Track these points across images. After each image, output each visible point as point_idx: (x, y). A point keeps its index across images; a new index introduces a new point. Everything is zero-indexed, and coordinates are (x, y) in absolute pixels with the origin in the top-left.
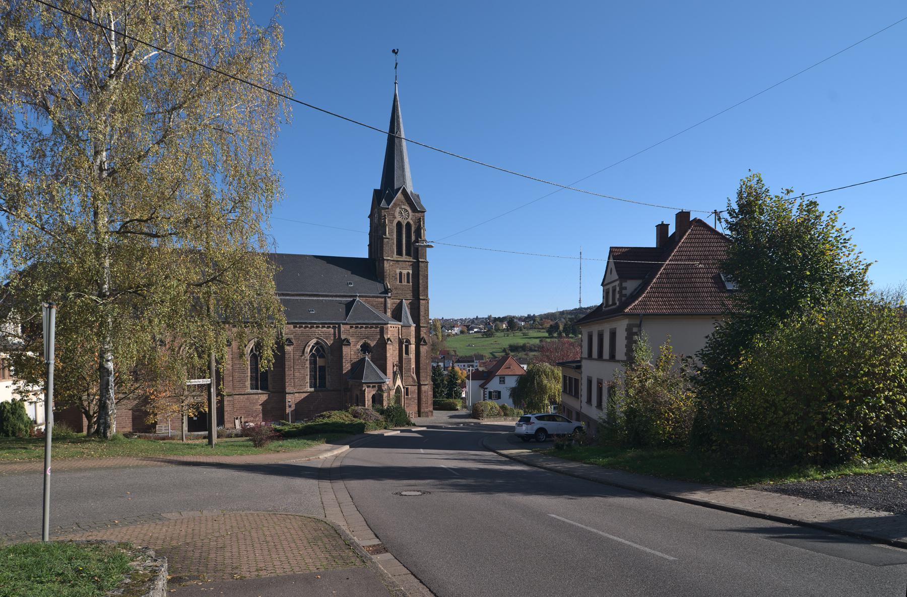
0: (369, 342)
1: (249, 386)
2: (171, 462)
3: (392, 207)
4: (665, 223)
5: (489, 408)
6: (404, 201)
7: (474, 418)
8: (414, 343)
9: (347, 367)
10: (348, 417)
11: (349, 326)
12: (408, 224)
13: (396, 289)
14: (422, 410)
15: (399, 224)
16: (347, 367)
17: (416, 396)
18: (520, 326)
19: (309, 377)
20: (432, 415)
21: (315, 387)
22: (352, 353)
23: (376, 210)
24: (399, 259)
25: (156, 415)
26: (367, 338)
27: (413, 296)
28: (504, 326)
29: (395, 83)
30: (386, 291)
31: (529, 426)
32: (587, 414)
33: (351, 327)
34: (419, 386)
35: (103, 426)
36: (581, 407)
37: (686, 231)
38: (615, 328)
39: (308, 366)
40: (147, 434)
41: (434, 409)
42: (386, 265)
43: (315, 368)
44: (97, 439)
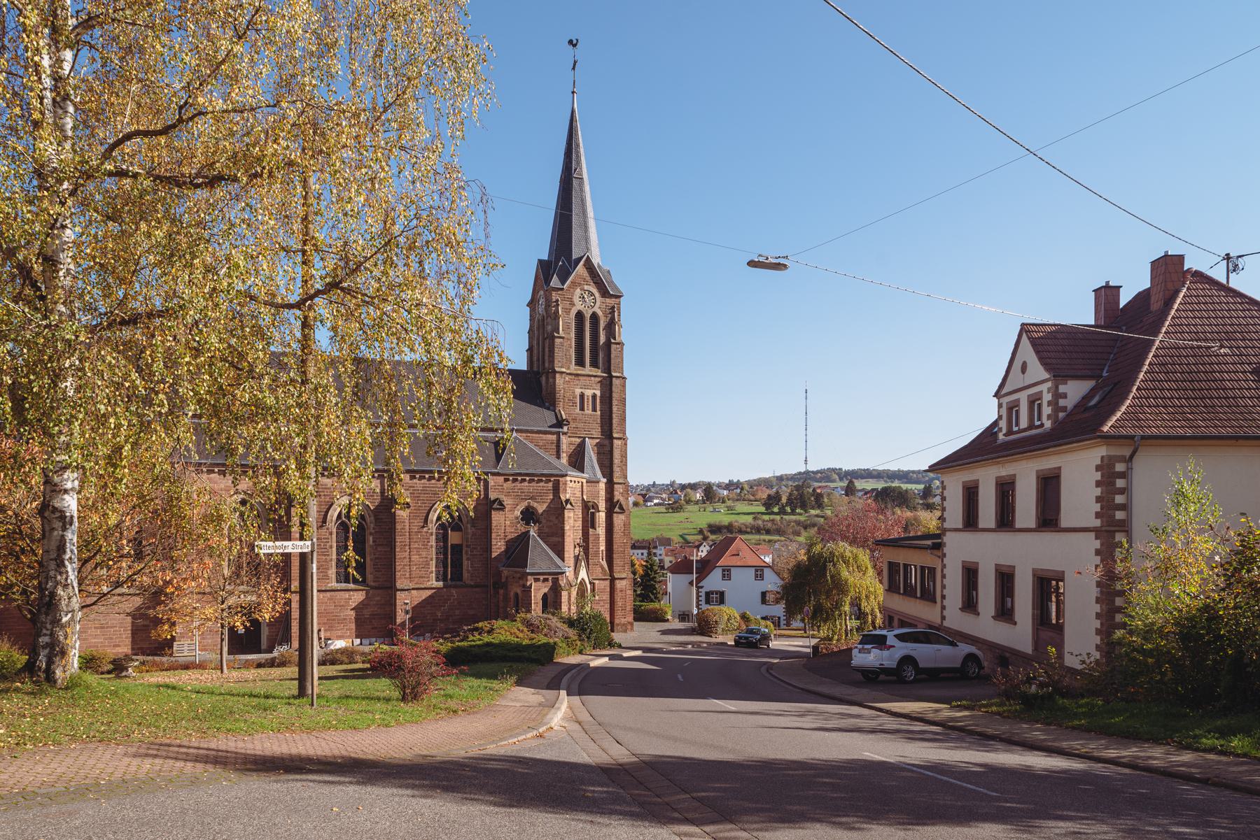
0: (535, 505)
1: (334, 576)
2: (220, 760)
3: (570, 287)
4: (1111, 284)
5: (726, 618)
6: (588, 278)
7: (702, 634)
8: (604, 509)
9: (498, 547)
10: (522, 631)
11: (502, 478)
12: (594, 317)
13: (574, 420)
14: (617, 621)
15: (580, 316)
16: (498, 547)
17: (606, 597)
18: (722, 496)
19: (434, 562)
20: (632, 629)
21: (445, 579)
22: (508, 523)
23: (542, 293)
24: (579, 372)
25: (174, 624)
26: (531, 498)
27: (603, 432)
28: (698, 495)
29: (573, 92)
30: (560, 423)
31: (886, 653)
32: (960, 630)
33: (506, 480)
34: (613, 580)
35: (47, 651)
36: (943, 618)
37: (1177, 292)
38: (1059, 468)
39: (434, 544)
40: (157, 659)
41: (636, 619)
42: (559, 380)
43: (445, 547)
44: (29, 686)
